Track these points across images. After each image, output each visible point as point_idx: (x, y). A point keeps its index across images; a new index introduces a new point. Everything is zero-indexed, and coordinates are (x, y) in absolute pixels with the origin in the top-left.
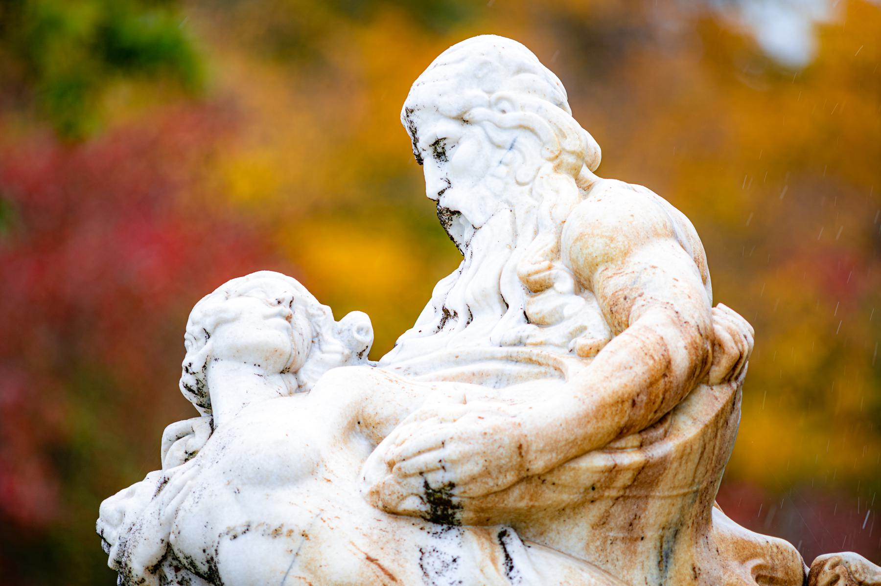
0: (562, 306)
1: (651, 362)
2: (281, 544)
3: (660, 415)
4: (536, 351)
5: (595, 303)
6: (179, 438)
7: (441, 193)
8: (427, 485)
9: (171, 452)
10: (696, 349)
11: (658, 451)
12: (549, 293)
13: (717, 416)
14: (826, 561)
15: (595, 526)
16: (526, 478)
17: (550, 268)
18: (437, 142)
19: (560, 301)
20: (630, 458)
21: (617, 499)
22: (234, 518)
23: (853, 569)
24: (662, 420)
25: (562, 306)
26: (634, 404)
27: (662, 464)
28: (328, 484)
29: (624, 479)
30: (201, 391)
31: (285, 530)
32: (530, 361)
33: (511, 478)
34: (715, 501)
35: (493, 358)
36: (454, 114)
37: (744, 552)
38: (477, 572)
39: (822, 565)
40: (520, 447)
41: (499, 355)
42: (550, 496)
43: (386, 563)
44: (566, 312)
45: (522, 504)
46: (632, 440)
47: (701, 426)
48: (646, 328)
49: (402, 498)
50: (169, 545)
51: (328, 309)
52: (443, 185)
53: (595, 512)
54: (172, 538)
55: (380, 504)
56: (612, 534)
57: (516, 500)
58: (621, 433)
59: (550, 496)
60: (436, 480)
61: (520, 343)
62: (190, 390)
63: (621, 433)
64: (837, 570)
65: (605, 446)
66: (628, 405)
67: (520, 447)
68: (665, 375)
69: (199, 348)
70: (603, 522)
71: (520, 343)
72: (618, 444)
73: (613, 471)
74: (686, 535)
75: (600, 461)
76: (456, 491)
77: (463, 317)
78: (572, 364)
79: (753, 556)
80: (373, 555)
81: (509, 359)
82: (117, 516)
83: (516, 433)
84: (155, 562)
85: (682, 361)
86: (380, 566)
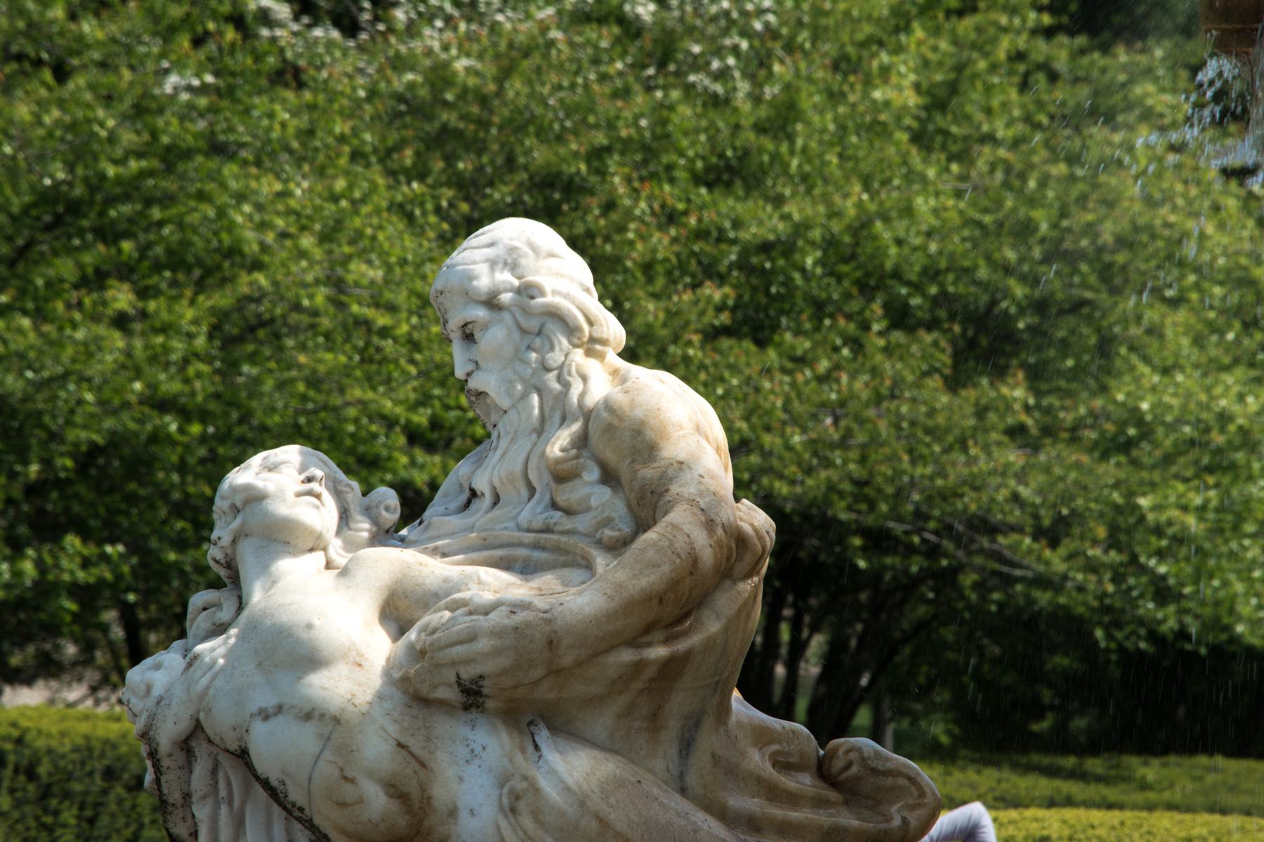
0: (589, 496)
1: (678, 561)
2: (310, 729)
3: (685, 610)
4: (564, 539)
5: (621, 495)
6: (205, 609)
7: (469, 374)
8: (458, 676)
9: (197, 622)
10: (721, 547)
11: (682, 646)
12: (577, 482)
13: (739, 610)
14: (839, 746)
15: (619, 717)
16: (556, 672)
17: (577, 457)
18: (466, 324)
19: (585, 491)
20: (659, 652)
21: (642, 690)
22: (266, 699)
23: (866, 755)
24: (686, 615)
25: (589, 496)
26: (661, 601)
27: (687, 656)
28: (358, 669)
29: (650, 673)
30: (231, 565)
31: (317, 713)
32: (558, 549)
33: (539, 672)
34: (736, 694)
35: (520, 544)
36: (484, 298)
37: (762, 737)
38: (506, 761)
39: (835, 750)
40: (551, 642)
41: (526, 541)
42: (578, 689)
43: (416, 749)
44: (593, 503)
45: (551, 696)
46: (658, 635)
47: (725, 620)
48: (674, 526)
49: (434, 687)
50: (198, 721)
51: (355, 484)
52: (470, 367)
53: (618, 703)
54: (202, 716)
55: (411, 690)
56: (637, 724)
57: (545, 693)
58: (648, 629)
59: (578, 689)
60: (467, 673)
61: (547, 530)
62: (217, 562)
63: (648, 629)
64: (852, 755)
65: (636, 640)
66: (655, 602)
67: (551, 642)
68: (691, 574)
69: (228, 524)
70: (628, 712)
71: (547, 530)
72: (645, 639)
73: (639, 666)
74: (708, 723)
75: (627, 656)
76: (486, 683)
77: (488, 499)
78: (601, 561)
79: (771, 742)
80: (403, 740)
81: (536, 546)
82: (143, 687)
83: (547, 629)
84: (184, 737)
85: (707, 556)
86: (411, 753)
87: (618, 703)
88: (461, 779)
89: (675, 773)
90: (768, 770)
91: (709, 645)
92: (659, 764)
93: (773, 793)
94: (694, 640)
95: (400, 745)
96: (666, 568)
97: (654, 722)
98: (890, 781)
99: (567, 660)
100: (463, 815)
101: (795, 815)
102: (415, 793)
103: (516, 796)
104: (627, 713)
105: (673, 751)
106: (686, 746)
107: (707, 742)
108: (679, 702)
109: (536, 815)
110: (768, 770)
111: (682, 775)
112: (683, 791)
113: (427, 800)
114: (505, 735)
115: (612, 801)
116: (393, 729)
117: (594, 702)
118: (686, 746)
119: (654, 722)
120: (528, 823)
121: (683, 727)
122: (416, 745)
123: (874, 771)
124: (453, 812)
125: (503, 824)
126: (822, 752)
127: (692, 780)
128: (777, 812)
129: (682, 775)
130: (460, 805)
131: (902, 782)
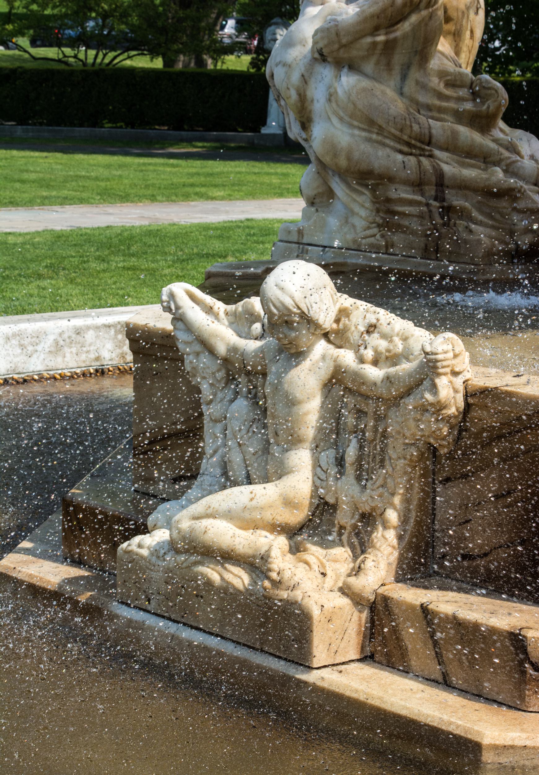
11: (392, 36)
20: (381, 38)
26: (378, 17)
27: (395, 40)
33: (336, 46)
43: (306, 77)
46: (383, 31)
53: (374, 59)
65: (375, 30)
66: (376, 18)
68: (392, 6)
75: (369, 40)
87: (374, 59)
88: (316, 88)
89: (399, 87)
90: (441, 87)
91: (405, 36)
92: (392, 83)
93: (440, 96)
94: (398, 34)
95: (303, 76)
96: (381, 4)
97: (389, 67)
98: (489, 92)
99: (344, 41)
100: (315, 101)
101: (445, 104)
102: (302, 94)
103: (331, 95)
104: (377, 63)
105: (398, 78)
106: (404, 77)
107: (414, 74)
108: (398, 59)
109: (336, 102)
110: (441, 87)
111: (401, 88)
112: (401, 94)
113: (305, 96)
114: (333, 71)
115: (359, 97)
116: (303, 69)
117: (365, 58)
118: (404, 77)
119: (389, 67)
120: (334, 105)
121: (402, 69)
122: (306, 75)
123: (484, 87)
124: (312, 101)
125: (327, 105)
126: (474, 78)
127: (406, 90)
128: (437, 102)
129: (401, 88)
130: (315, 98)
131: (489, 92)
